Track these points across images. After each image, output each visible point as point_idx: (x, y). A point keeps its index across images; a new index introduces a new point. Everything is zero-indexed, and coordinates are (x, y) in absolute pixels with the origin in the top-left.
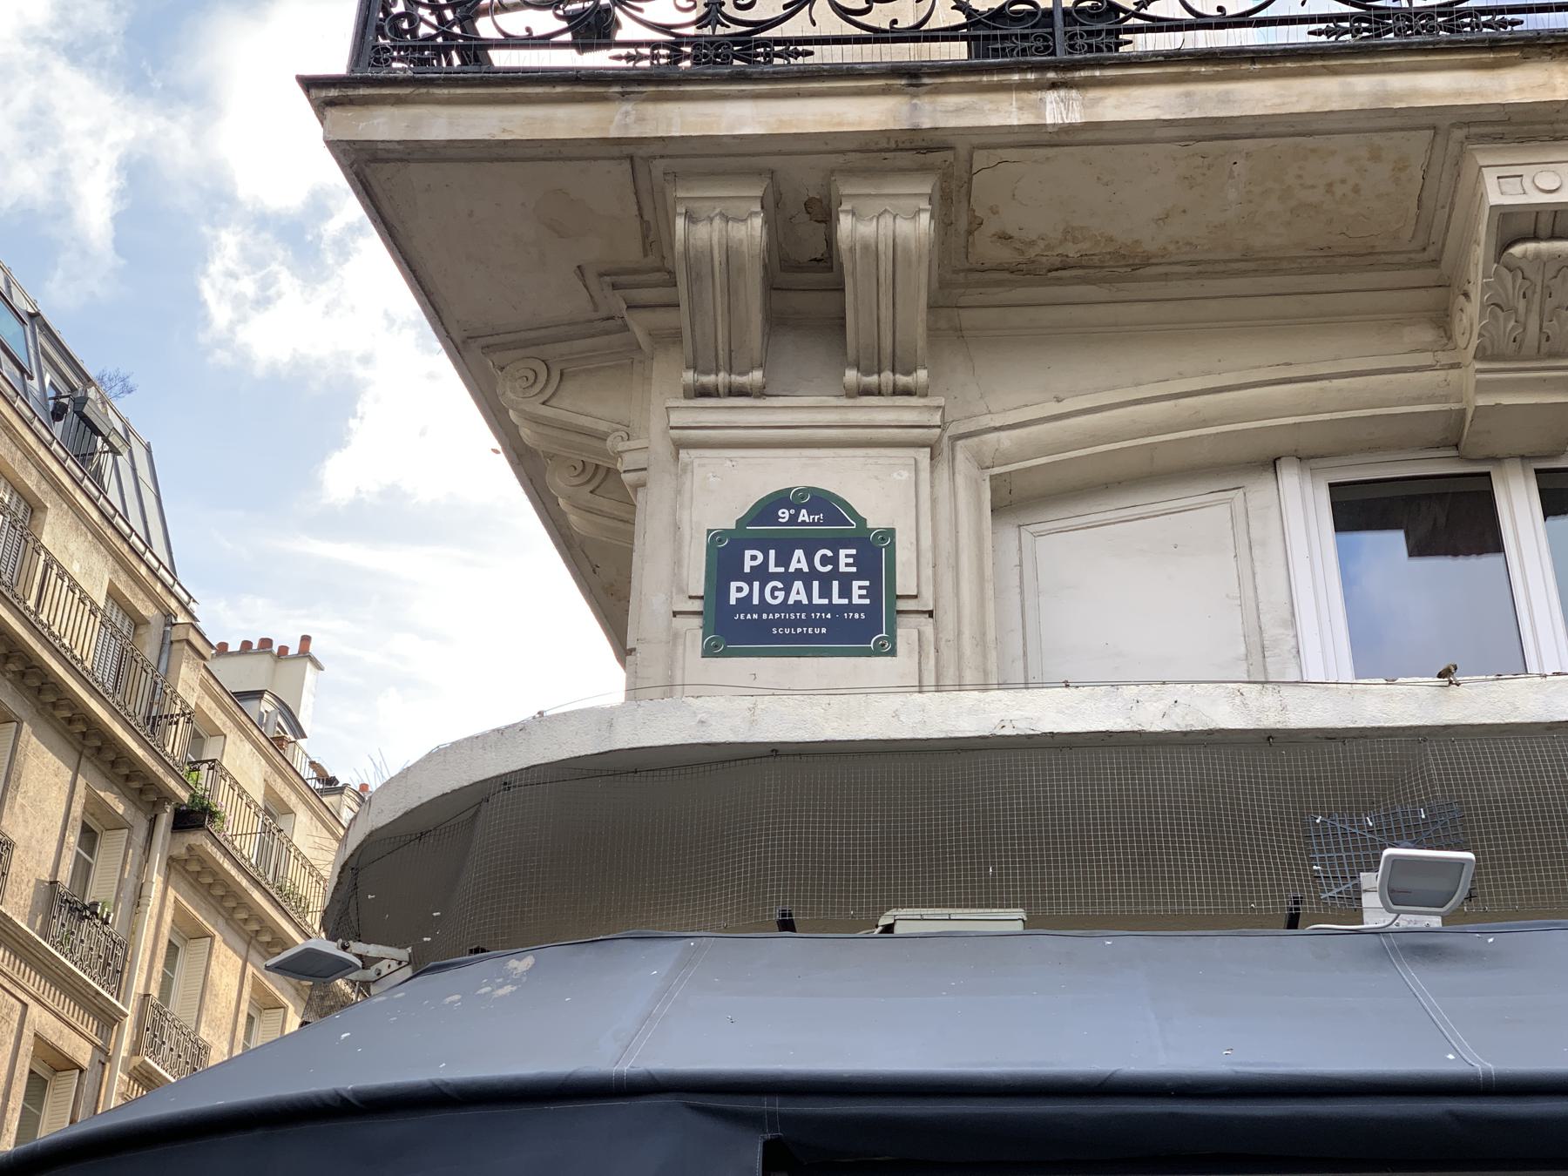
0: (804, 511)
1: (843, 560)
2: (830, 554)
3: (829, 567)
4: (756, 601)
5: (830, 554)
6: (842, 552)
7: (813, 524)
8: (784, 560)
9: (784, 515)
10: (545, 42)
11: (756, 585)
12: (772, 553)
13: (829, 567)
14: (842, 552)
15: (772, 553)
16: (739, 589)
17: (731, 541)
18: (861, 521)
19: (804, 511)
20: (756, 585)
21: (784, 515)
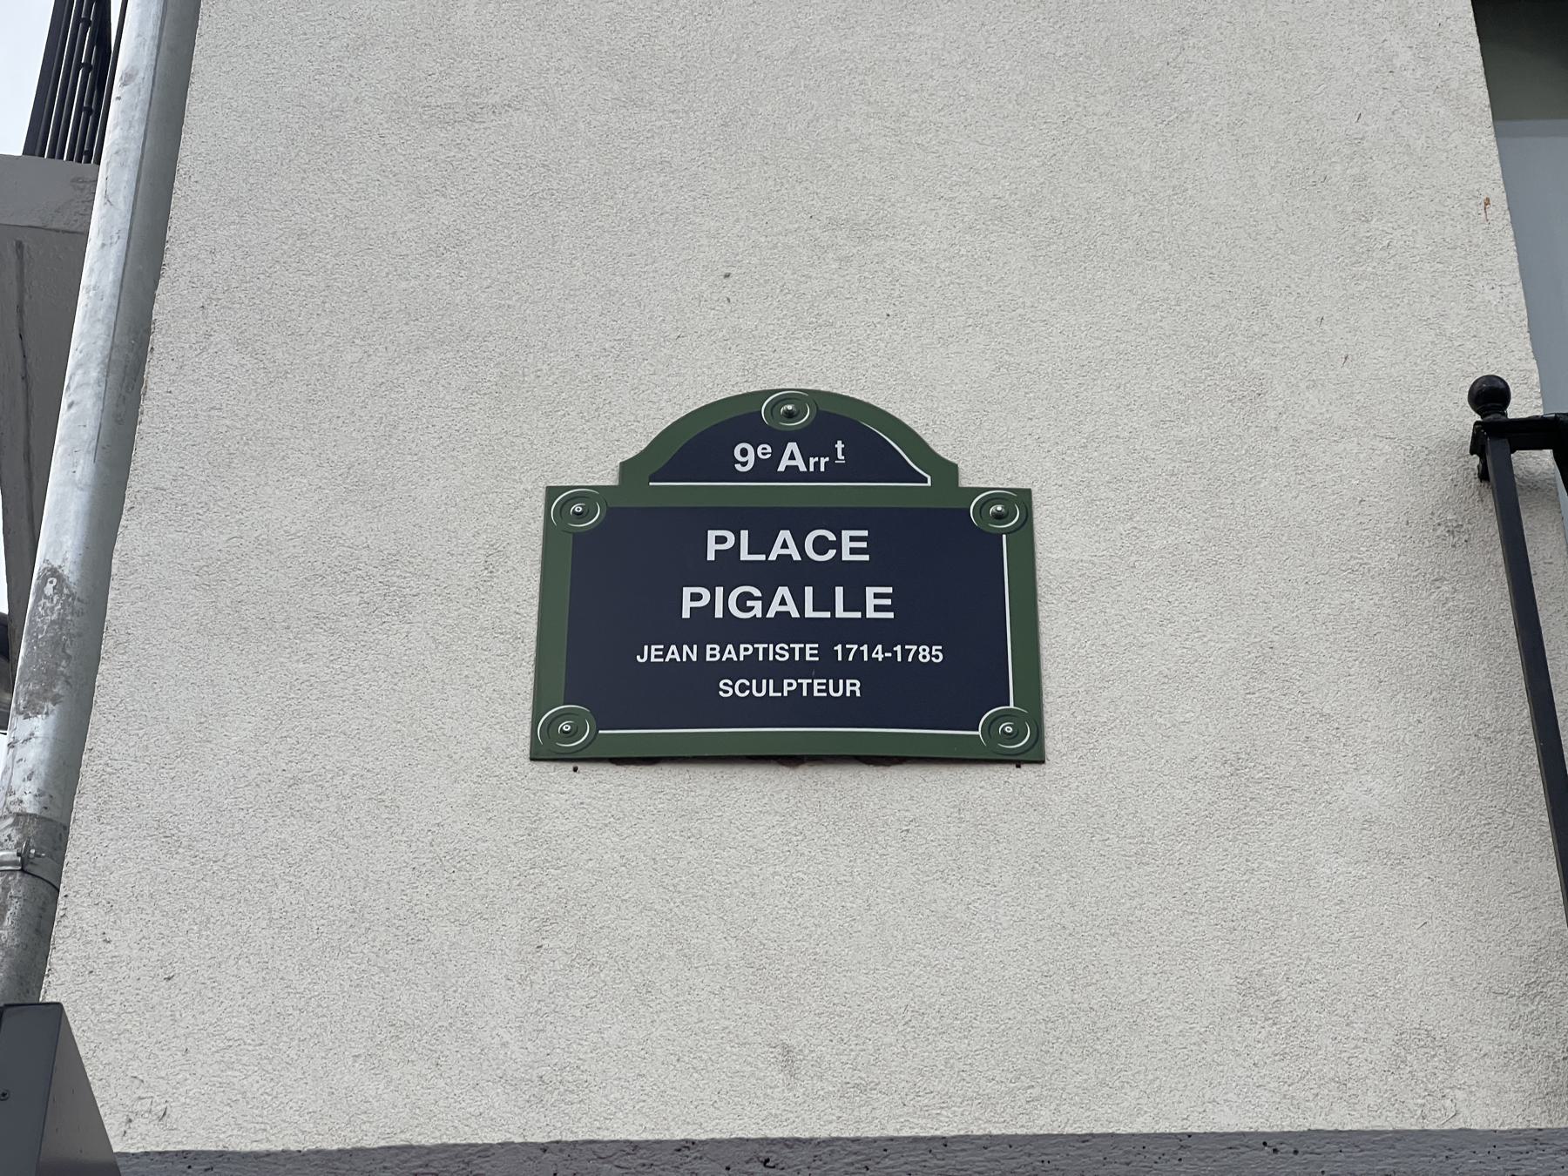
0: (792, 447)
1: (847, 545)
2: (832, 537)
3: (832, 553)
4: (719, 614)
5: (832, 537)
6: (846, 534)
7: (816, 476)
8: (761, 543)
9: (747, 456)
10: (732, 670)
11: (719, 591)
12: (744, 534)
13: (832, 553)
14: (846, 534)
15: (744, 534)
16: (746, 649)
17: (610, 513)
18: (947, 471)
19: (792, 447)
20: (719, 591)
21: (747, 456)
